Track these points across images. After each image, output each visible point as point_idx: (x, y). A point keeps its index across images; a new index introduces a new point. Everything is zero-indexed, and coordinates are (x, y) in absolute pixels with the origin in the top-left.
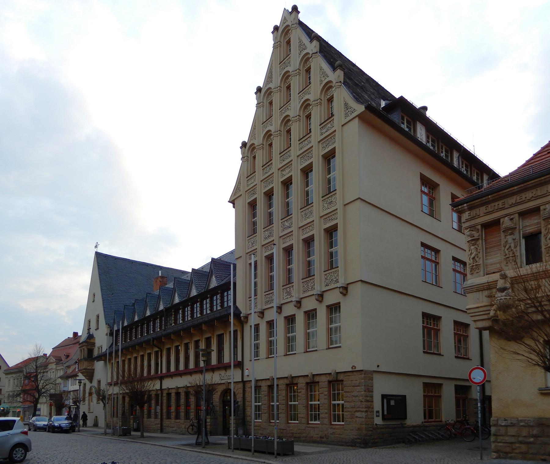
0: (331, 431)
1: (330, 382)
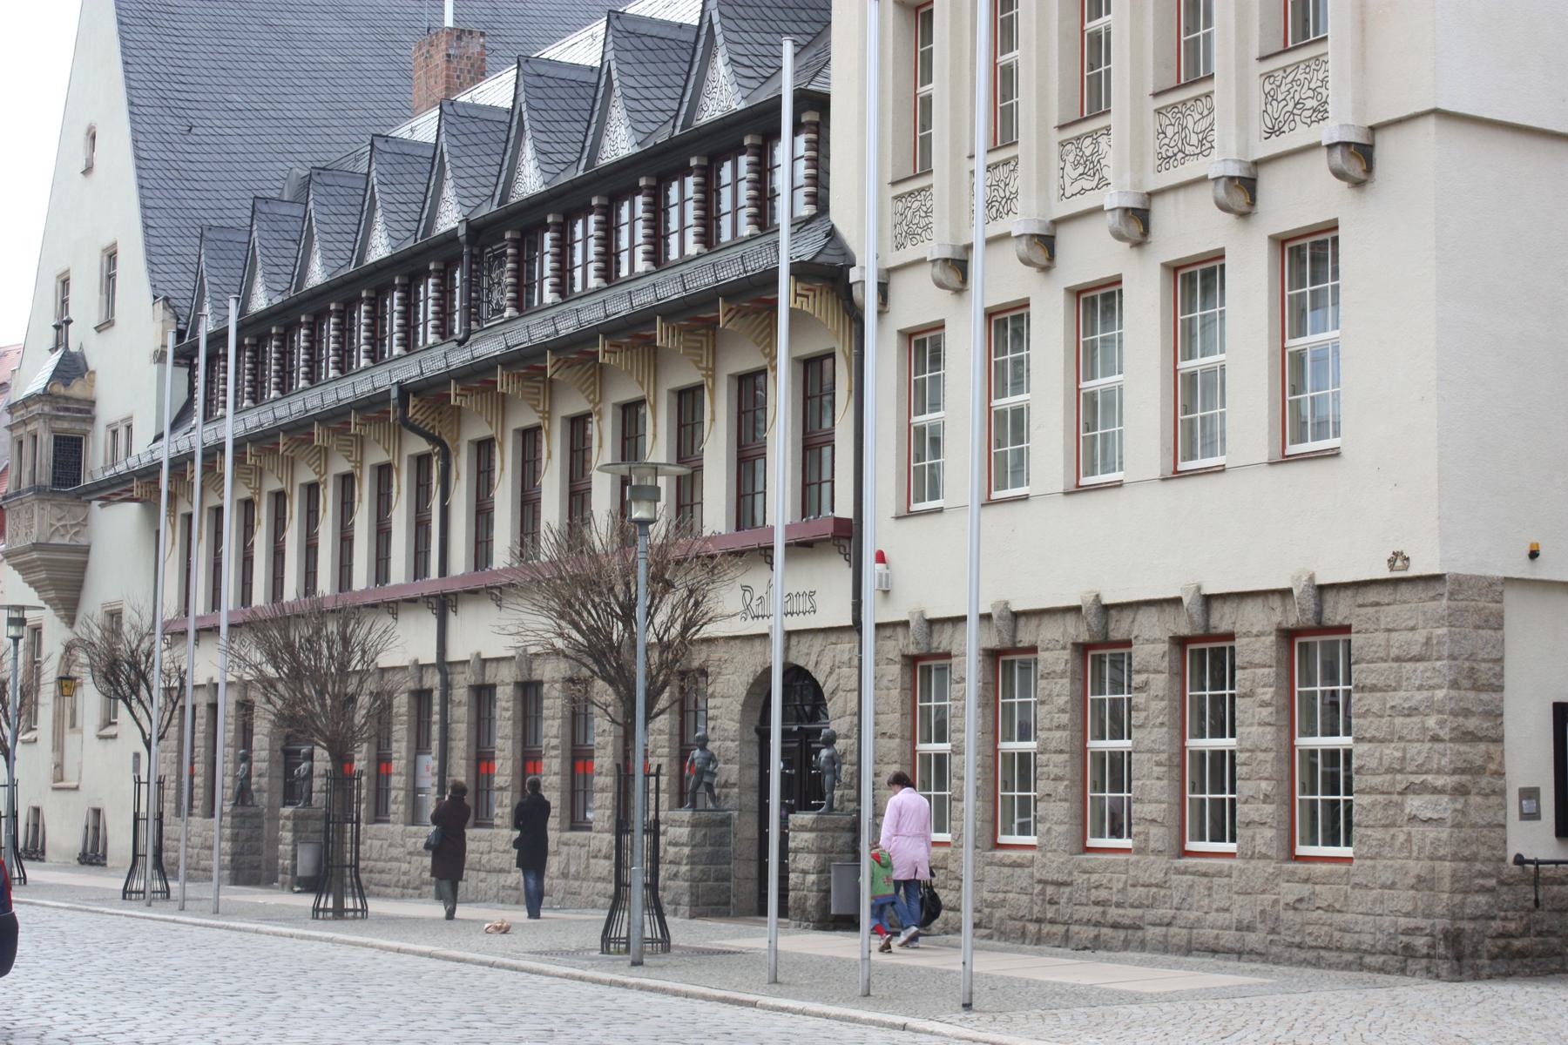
0: (1290, 891)
1: (1288, 635)
